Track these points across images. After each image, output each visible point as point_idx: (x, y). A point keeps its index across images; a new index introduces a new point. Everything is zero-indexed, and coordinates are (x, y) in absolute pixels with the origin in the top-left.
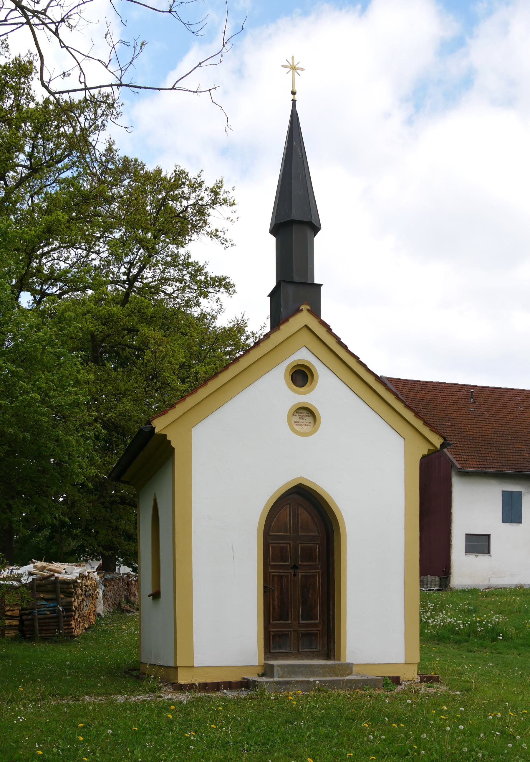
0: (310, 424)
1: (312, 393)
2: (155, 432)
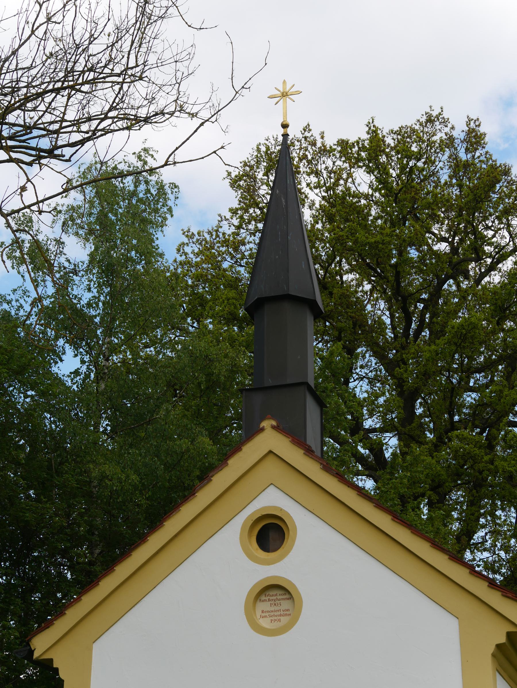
0: (288, 613)
1: (286, 560)
2: (34, 657)
